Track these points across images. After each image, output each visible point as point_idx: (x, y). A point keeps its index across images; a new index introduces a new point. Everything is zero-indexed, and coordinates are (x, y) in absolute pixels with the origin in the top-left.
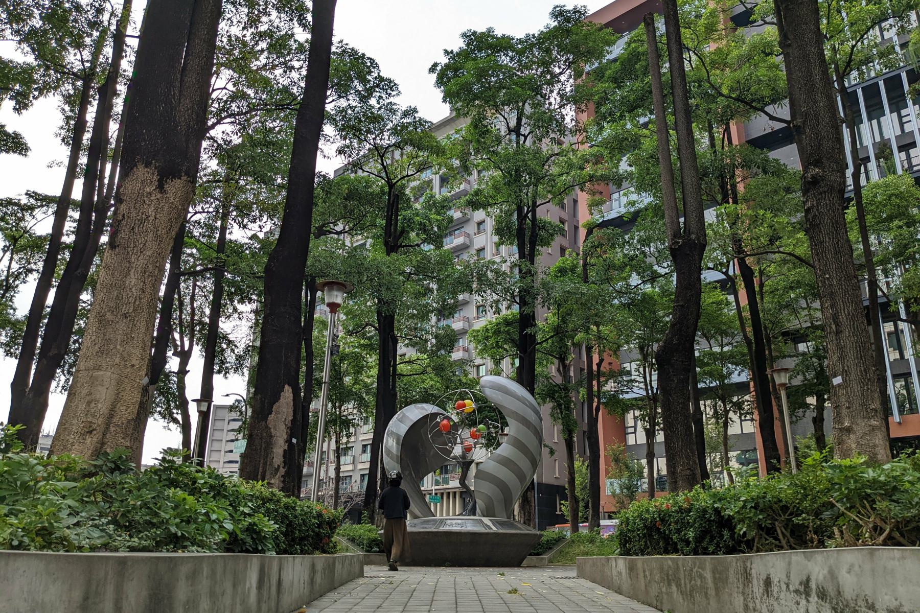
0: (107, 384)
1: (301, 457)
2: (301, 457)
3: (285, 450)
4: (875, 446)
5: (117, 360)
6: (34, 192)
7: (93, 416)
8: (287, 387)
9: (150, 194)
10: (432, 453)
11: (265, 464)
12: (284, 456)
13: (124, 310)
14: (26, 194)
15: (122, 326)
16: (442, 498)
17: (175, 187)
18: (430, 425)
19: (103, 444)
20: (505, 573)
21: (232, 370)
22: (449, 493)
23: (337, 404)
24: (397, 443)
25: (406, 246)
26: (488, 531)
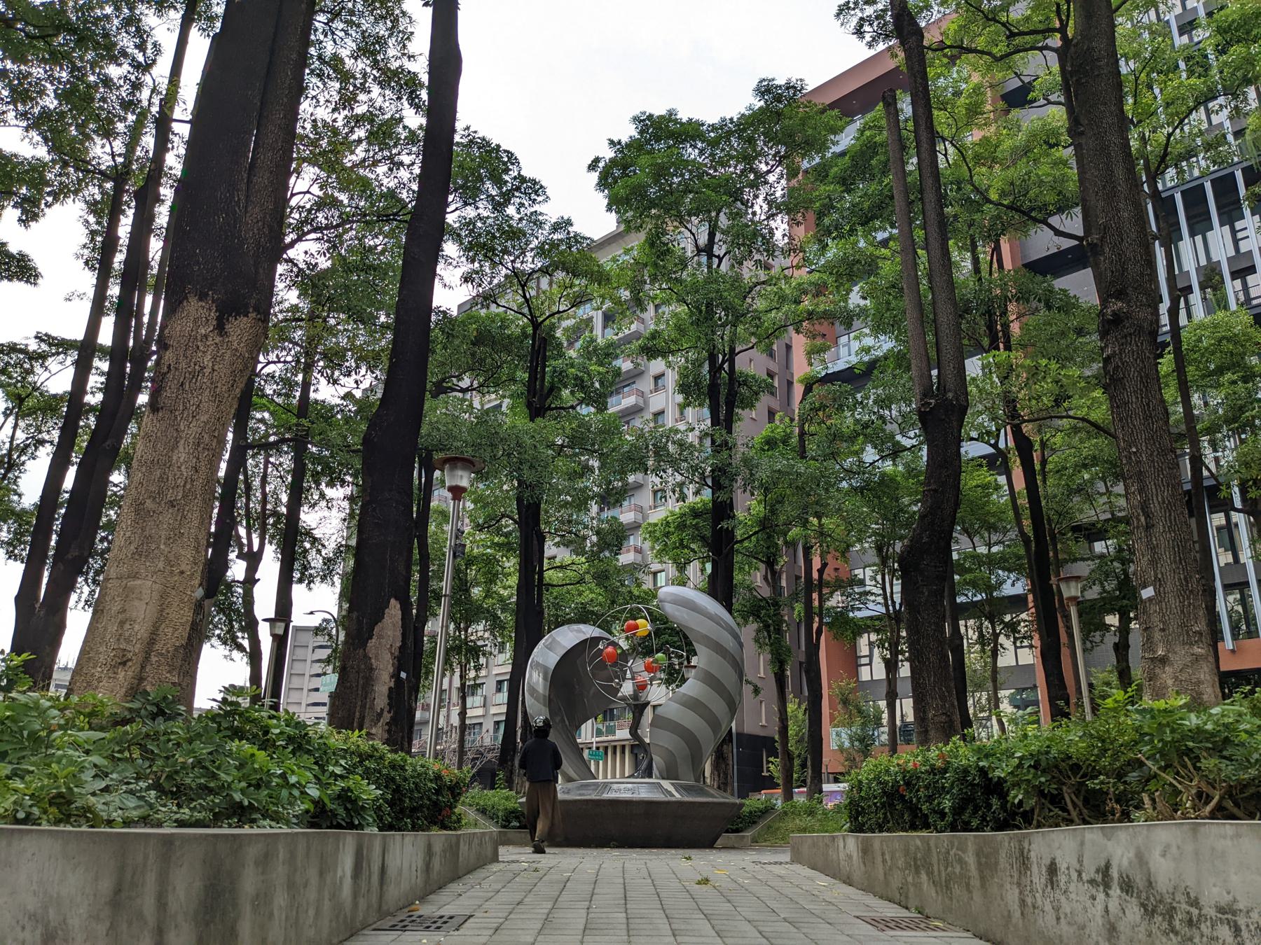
0: (146, 597)
1: (413, 698)
2: (413, 698)
3: (390, 689)
4: (1199, 682)
5: (161, 565)
6: (46, 335)
7: (128, 641)
8: (393, 601)
9: (206, 336)
10: (592, 692)
11: (363, 706)
12: (390, 697)
13: (170, 496)
14: (36, 337)
15: (168, 517)
16: (606, 753)
17: (240, 327)
18: (589, 654)
19: (141, 679)
20: (693, 857)
21: (319, 578)
22: (615, 747)
23: (462, 625)
24: (545, 679)
25: (556, 408)
26: (669, 798)
